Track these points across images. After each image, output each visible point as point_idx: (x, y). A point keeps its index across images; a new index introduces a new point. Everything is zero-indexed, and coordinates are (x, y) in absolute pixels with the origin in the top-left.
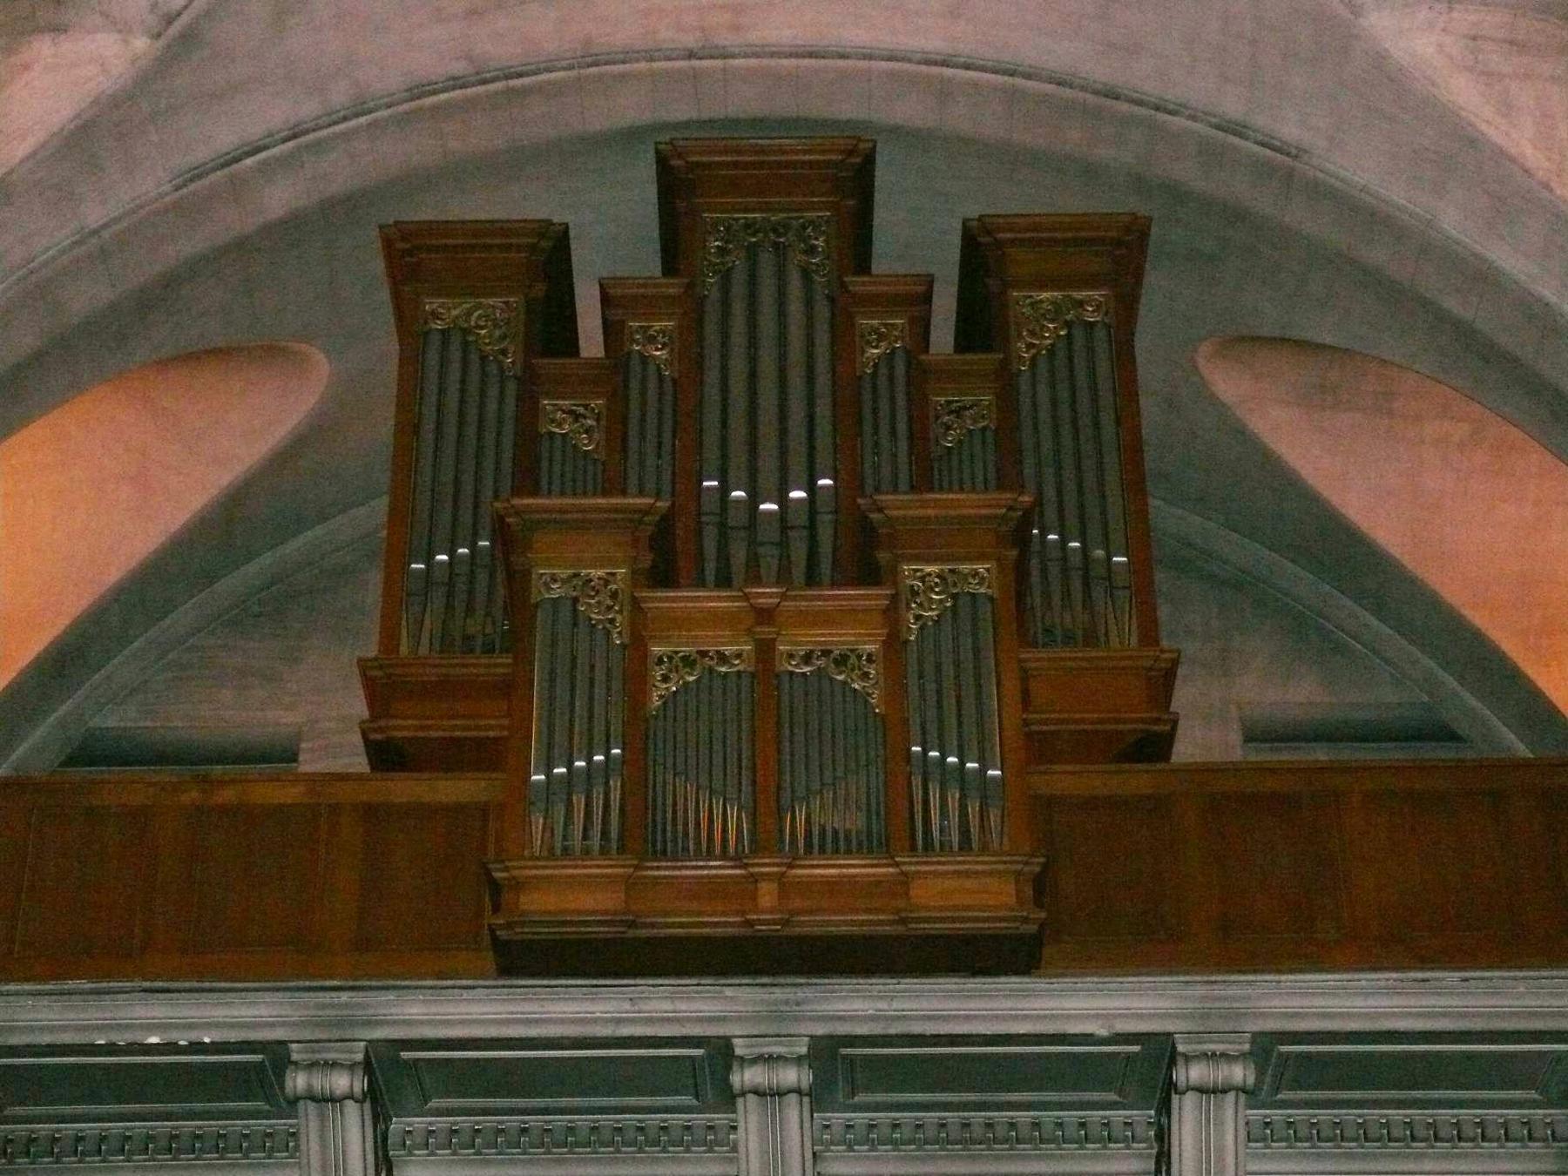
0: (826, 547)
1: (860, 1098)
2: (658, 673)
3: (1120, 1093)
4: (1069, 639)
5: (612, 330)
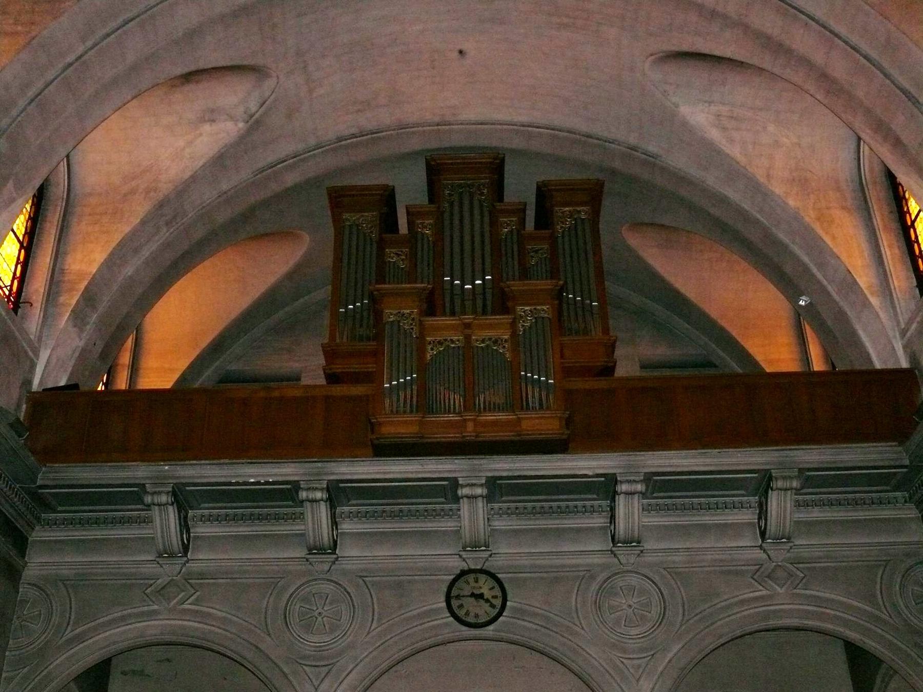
0: (489, 303)
1: (202, 505)
2: (429, 347)
3: (598, 495)
4: (577, 333)
5: (411, 224)
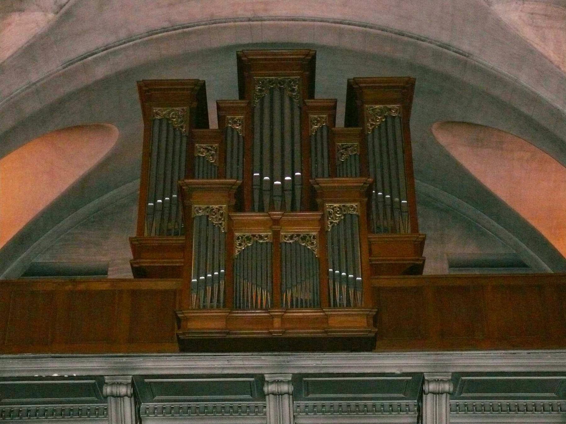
0: (298, 197)
1: (310, 396)
2: (238, 243)
3: (404, 394)
4: (386, 230)
5: (221, 119)
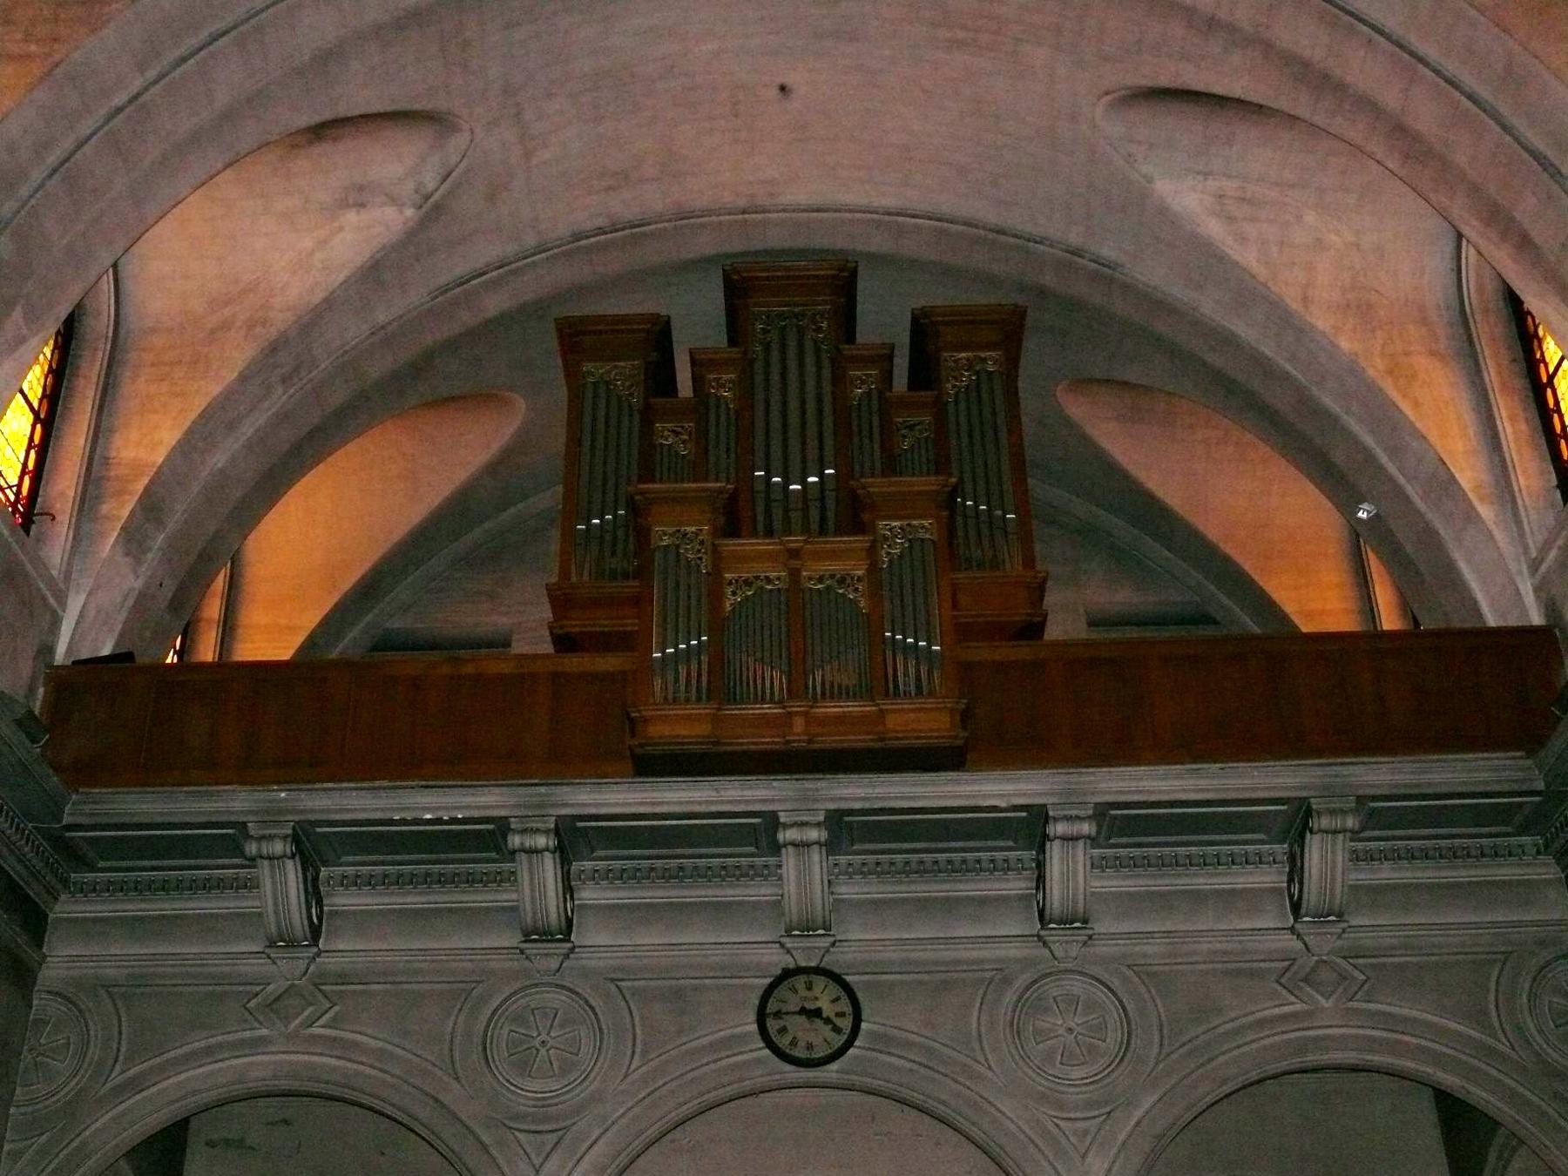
0: (830, 515)
1: (344, 859)
2: (729, 590)
3: (1016, 841)
4: (980, 566)
5: (697, 380)
